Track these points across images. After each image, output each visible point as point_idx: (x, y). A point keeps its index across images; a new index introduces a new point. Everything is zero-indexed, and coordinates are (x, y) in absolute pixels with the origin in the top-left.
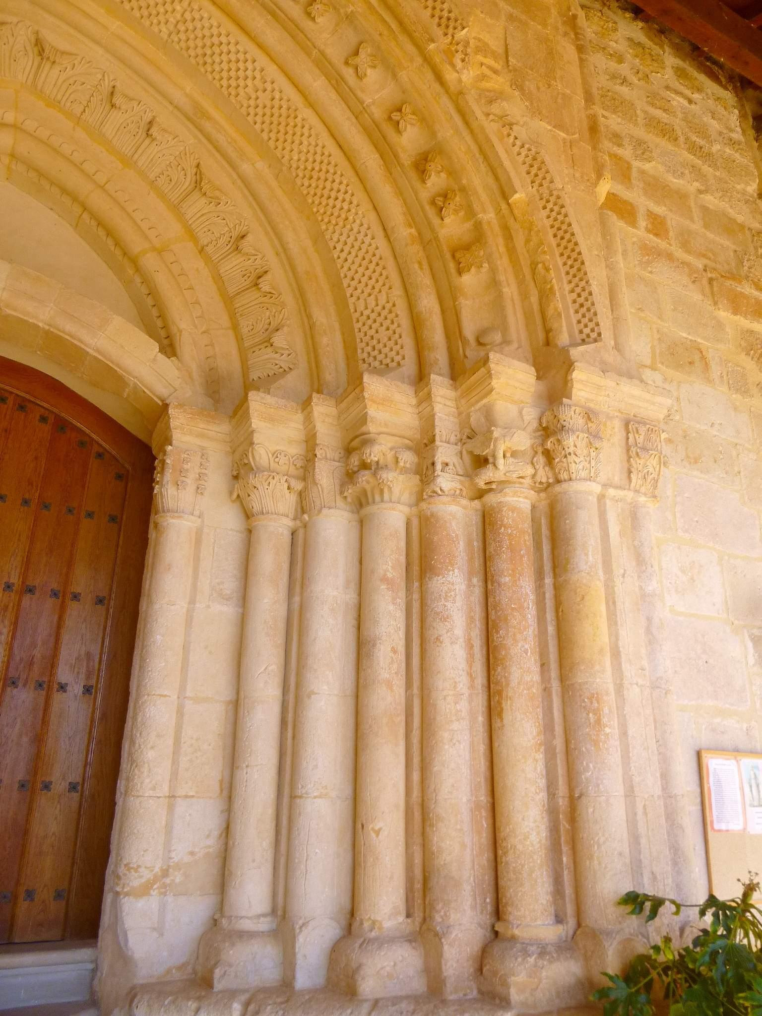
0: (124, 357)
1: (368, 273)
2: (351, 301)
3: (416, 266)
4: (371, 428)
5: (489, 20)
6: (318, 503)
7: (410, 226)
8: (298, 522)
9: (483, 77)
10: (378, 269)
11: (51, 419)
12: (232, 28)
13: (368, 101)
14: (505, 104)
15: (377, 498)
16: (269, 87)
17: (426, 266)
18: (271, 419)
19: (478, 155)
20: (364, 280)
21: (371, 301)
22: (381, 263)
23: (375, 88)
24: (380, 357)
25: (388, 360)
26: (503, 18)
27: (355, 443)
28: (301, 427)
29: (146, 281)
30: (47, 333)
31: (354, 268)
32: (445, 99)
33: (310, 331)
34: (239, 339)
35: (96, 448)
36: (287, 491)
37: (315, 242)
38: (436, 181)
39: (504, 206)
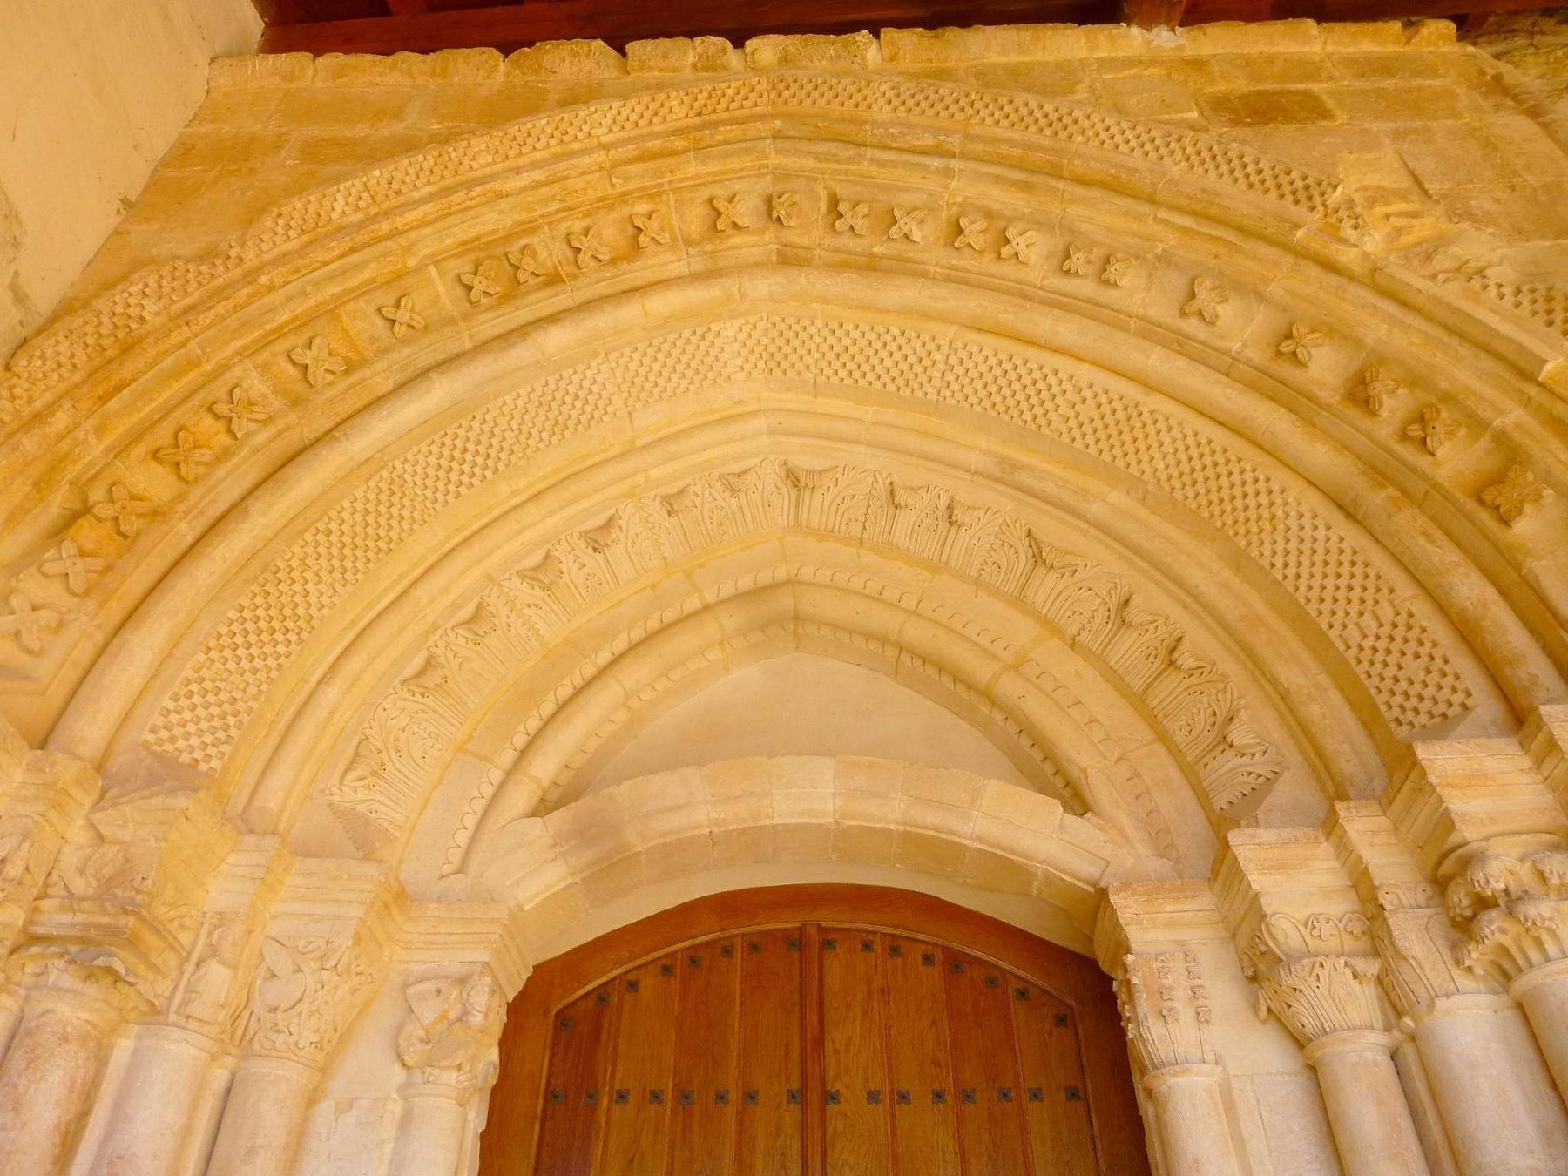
0: (1015, 838)
1: (1343, 582)
2: (1334, 634)
3: (1422, 541)
4: (1468, 833)
5: (1369, 157)
6: (1421, 992)
7: (1381, 486)
8: (1396, 1034)
9: (1398, 232)
10: (1359, 570)
11: (938, 955)
12: (1014, 347)
13: (1235, 346)
14: (1455, 250)
15: (1535, 955)
16: (1088, 393)
17: (1438, 534)
18: (1281, 867)
19: (1446, 339)
20: (1341, 594)
21: (1368, 622)
22: (1359, 559)
23: (1240, 327)
24: (1424, 707)
25: (1442, 707)
26: (1387, 141)
27: (1446, 869)
28: (1336, 864)
29: (1010, 714)
30: (905, 836)
31: (1316, 583)
32: (1353, 290)
33: (1285, 703)
34: (1174, 751)
35: (1013, 985)
36: (1355, 984)
37: (1237, 569)
38: (1394, 405)
39: (1532, 390)
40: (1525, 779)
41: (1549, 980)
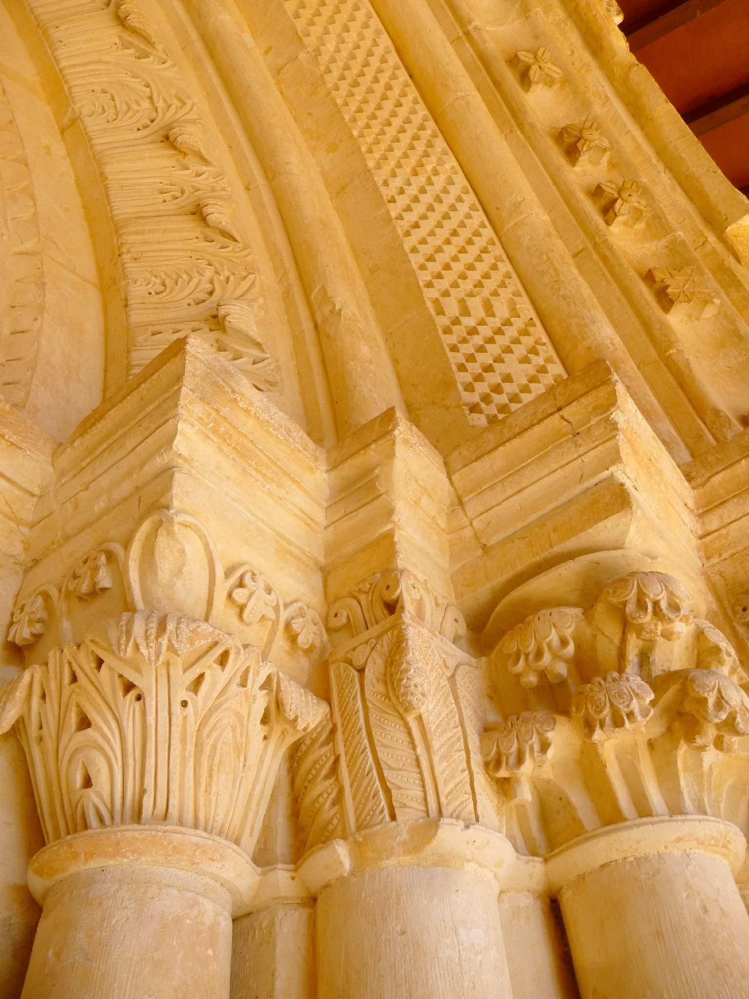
6: (408, 793)
18: (243, 453)
19: (654, 160)
28: (320, 516)
36: (257, 730)
41: (677, 853)
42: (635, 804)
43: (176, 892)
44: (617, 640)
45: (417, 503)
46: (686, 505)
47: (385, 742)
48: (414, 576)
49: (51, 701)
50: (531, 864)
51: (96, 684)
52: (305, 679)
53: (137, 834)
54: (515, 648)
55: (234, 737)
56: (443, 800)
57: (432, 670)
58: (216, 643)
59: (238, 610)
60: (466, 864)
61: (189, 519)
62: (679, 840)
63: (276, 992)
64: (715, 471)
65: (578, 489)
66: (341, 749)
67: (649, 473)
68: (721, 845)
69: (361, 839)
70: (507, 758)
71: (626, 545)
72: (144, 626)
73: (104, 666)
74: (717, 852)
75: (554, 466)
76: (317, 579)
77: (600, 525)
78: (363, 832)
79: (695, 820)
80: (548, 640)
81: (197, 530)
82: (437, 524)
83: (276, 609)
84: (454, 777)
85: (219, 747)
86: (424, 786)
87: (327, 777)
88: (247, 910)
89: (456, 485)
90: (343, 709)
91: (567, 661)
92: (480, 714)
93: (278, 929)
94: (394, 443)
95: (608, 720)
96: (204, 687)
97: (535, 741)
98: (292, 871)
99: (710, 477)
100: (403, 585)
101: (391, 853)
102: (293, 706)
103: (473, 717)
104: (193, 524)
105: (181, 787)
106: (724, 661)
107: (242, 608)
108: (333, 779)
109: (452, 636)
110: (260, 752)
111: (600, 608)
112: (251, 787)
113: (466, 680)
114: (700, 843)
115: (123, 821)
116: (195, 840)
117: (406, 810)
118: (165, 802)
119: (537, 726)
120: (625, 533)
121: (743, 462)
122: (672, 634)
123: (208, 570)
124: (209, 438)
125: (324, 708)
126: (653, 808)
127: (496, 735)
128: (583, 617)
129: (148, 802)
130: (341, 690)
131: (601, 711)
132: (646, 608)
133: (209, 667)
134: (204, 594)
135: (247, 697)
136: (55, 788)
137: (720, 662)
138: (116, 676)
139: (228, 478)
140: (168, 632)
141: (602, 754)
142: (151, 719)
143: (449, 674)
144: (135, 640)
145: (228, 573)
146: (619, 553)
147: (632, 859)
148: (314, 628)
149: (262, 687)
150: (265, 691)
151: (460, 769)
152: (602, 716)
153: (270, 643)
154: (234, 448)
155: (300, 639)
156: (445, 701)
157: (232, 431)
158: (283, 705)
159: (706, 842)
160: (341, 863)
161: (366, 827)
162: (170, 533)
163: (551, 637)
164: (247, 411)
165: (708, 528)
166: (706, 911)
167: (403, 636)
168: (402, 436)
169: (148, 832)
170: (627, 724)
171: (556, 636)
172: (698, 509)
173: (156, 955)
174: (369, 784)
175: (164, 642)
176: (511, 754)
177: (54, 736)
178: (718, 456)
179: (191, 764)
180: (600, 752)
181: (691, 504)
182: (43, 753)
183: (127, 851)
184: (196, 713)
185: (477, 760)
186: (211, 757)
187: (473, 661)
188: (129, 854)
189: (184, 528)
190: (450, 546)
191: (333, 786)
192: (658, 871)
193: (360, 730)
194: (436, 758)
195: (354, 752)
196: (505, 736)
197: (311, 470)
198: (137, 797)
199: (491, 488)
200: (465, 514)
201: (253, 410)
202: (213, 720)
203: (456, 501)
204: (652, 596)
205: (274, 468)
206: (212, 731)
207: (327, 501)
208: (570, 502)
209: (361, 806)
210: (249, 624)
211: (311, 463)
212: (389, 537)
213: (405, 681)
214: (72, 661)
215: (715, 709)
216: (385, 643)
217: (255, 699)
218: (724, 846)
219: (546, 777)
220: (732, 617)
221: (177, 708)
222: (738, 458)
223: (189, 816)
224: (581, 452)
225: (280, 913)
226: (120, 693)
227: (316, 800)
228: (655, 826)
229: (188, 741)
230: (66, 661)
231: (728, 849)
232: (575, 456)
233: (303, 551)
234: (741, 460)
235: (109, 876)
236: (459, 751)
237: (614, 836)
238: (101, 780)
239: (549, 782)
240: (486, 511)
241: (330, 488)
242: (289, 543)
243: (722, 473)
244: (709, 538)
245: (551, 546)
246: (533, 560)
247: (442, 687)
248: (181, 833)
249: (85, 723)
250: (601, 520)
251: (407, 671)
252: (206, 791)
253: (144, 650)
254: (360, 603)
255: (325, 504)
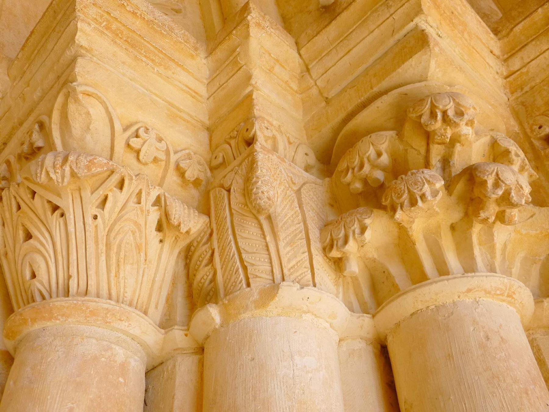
6: (260, 268)
8: (178, 335)
15: (452, 260)
18: (132, 43)
28: (203, 90)
36: (154, 236)
40: (491, 60)
41: (468, 300)
42: (438, 269)
43: (94, 341)
44: (423, 151)
45: (271, 70)
46: (491, 52)
47: (244, 235)
48: (268, 121)
49: (8, 226)
50: (361, 318)
51: (33, 209)
52: (196, 204)
53: (63, 304)
54: (346, 166)
55: (135, 239)
56: (286, 271)
57: (280, 184)
58: (112, 172)
59: (136, 155)
60: (303, 315)
61: (90, 89)
62: (469, 291)
63: (174, 408)
64: (517, 22)
65: (391, 42)
66: (215, 245)
67: (453, 24)
68: (506, 294)
69: (227, 302)
70: (337, 241)
71: (429, 78)
72: (53, 160)
73: (36, 195)
74: (504, 301)
75: (372, 27)
76: (204, 136)
77: (407, 64)
78: (228, 298)
79: (483, 276)
80: (367, 155)
81: (98, 98)
82: (290, 87)
83: (167, 153)
84: (296, 257)
85: (123, 246)
86: (271, 263)
87: (206, 265)
88: (159, 361)
89: (304, 57)
90: (217, 217)
91: (384, 169)
92: (322, 216)
93: (177, 369)
94: (248, 27)
95: (406, 203)
96: (108, 205)
97: (356, 227)
98: (186, 330)
99: (512, 29)
100: (257, 126)
101: (246, 308)
102: (176, 216)
103: (316, 218)
104: (93, 93)
105: (97, 273)
106: (513, 161)
107: (138, 152)
108: (210, 266)
109: (303, 165)
110: (158, 251)
111: (408, 127)
112: (153, 275)
113: (311, 193)
114: (487, 292)
115: (57, 296)
116: (106, 306)
117: (258, 279)
118: (85, 284)
119: (358, 216)
120: (427, 68)
121: (540, 10)
122: (460, 136)
123: (109, 127)
124: (104, 33)
125: (204, 219)
126: (450, 270)
127: (330, 227)
128: (397, 137)
129: (73, 284)
130: (216, 205)
131: (401, 196)
132: (436, 117)
133: (111, 190)
134: (108, 145)
135: (142, 211)
136: (16, 284)
137: (509, 162)
138: (45, 202)
139: (124, 63)
140: (69, 162)
141: (412, 235)
142: (71, 228)
143: (295, 188)
144: (46, 169)
145: (125, 130)
146: (423, 84)
147: (433, 307)
148: (199, 167)
149: (154, 205)
150: (156, 208)
151: (301, 251)
152: (402, 200)
153: (163, 178)
154: (125, 40)
155: (187, 175)
156: (291, 205)
157: (122, 28)
158: (169, 215)
159: (493, 292)
160: (213, 319)
161: (231, 293)
162: (77, 100)
163: (369, 152)
164: (134, 13)
165: (512, 69)
166: (488, 338)
167: (254, 160)
168: (254, 21)
169: (71, 302)
170: (420, 203)
171: (376, 152)
172: (504, 55)
173: (78, 379)
174: (232, 265)
175: (67, 169)
176: (339, 239)
177: (12, 248)
178: (520, 10)
179: (103, 258)
180: (410, 233)
181: (497, 52)
182: (9, 263)
183: (58, 315)
184: (104, 223)
185: (316, 248)
186: (118, 253)
187: (319, 181)
188: (59, 317)
189: (87, 97)
190: (303, 103)
191: (210, 270)
192: (452, 313)
193: (228, 229)
194: (281, 244)
195: (223, 246)
196: (336, 227)
197: (192, 56)
198: (66, 282)
199: (328, 54)
200: (311, 77)
201: (139, 13)
202: (117, 228)
203: (305, 69)
204: (441, 107)
205: (161, 55)
206: (116, 235)
207: (207, 79)
208: (386, 53)
209: (228, 280)
210: (145, 164)
211: (193, 53)
212: (249, 96)
213: (255, 190)
214: (16, 196)
215: (493, 188)
216: (243, 167)
217: (148, 213)
218: (508, 296)
219: (371, 256)
220: (529, 134)
221: (89, 220)
222: (536, 8)
223: (104, 291)
224: (392, 12)
225: (179, 359)
226: (49, 213)
227: (200, 282)
228: (450, 281)
229: (100, 242)
230: (12, 197)
231: (513, 298)
232: (388, 16)
233: (191, 116)
234: (538, 9)
235: (48, 333)
236: (301, 239)
237: (418, 291)
238: (42, 273)
239: (374, 260)
240: (326, 72)
241: (209, 70)
242: (179, 110)
243: (523, 23)
244: (513, 77)
245: (372, 88)
246: (359, 101)
247: (289, 196)
248: (95, 302)
249: (29, 236)
250: (407, 60)
251: (256, 182)
252: (116, 276)
253: (52, 175)
254: (231, 147)
255: (206, 82)
